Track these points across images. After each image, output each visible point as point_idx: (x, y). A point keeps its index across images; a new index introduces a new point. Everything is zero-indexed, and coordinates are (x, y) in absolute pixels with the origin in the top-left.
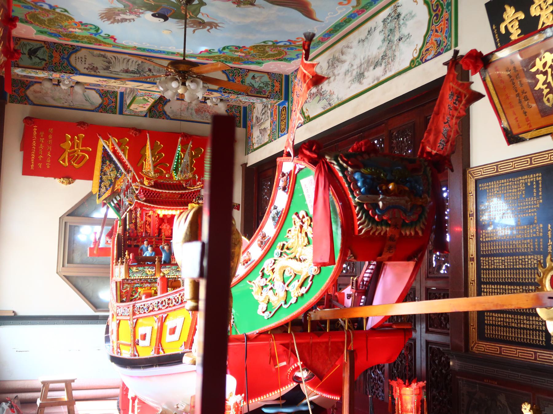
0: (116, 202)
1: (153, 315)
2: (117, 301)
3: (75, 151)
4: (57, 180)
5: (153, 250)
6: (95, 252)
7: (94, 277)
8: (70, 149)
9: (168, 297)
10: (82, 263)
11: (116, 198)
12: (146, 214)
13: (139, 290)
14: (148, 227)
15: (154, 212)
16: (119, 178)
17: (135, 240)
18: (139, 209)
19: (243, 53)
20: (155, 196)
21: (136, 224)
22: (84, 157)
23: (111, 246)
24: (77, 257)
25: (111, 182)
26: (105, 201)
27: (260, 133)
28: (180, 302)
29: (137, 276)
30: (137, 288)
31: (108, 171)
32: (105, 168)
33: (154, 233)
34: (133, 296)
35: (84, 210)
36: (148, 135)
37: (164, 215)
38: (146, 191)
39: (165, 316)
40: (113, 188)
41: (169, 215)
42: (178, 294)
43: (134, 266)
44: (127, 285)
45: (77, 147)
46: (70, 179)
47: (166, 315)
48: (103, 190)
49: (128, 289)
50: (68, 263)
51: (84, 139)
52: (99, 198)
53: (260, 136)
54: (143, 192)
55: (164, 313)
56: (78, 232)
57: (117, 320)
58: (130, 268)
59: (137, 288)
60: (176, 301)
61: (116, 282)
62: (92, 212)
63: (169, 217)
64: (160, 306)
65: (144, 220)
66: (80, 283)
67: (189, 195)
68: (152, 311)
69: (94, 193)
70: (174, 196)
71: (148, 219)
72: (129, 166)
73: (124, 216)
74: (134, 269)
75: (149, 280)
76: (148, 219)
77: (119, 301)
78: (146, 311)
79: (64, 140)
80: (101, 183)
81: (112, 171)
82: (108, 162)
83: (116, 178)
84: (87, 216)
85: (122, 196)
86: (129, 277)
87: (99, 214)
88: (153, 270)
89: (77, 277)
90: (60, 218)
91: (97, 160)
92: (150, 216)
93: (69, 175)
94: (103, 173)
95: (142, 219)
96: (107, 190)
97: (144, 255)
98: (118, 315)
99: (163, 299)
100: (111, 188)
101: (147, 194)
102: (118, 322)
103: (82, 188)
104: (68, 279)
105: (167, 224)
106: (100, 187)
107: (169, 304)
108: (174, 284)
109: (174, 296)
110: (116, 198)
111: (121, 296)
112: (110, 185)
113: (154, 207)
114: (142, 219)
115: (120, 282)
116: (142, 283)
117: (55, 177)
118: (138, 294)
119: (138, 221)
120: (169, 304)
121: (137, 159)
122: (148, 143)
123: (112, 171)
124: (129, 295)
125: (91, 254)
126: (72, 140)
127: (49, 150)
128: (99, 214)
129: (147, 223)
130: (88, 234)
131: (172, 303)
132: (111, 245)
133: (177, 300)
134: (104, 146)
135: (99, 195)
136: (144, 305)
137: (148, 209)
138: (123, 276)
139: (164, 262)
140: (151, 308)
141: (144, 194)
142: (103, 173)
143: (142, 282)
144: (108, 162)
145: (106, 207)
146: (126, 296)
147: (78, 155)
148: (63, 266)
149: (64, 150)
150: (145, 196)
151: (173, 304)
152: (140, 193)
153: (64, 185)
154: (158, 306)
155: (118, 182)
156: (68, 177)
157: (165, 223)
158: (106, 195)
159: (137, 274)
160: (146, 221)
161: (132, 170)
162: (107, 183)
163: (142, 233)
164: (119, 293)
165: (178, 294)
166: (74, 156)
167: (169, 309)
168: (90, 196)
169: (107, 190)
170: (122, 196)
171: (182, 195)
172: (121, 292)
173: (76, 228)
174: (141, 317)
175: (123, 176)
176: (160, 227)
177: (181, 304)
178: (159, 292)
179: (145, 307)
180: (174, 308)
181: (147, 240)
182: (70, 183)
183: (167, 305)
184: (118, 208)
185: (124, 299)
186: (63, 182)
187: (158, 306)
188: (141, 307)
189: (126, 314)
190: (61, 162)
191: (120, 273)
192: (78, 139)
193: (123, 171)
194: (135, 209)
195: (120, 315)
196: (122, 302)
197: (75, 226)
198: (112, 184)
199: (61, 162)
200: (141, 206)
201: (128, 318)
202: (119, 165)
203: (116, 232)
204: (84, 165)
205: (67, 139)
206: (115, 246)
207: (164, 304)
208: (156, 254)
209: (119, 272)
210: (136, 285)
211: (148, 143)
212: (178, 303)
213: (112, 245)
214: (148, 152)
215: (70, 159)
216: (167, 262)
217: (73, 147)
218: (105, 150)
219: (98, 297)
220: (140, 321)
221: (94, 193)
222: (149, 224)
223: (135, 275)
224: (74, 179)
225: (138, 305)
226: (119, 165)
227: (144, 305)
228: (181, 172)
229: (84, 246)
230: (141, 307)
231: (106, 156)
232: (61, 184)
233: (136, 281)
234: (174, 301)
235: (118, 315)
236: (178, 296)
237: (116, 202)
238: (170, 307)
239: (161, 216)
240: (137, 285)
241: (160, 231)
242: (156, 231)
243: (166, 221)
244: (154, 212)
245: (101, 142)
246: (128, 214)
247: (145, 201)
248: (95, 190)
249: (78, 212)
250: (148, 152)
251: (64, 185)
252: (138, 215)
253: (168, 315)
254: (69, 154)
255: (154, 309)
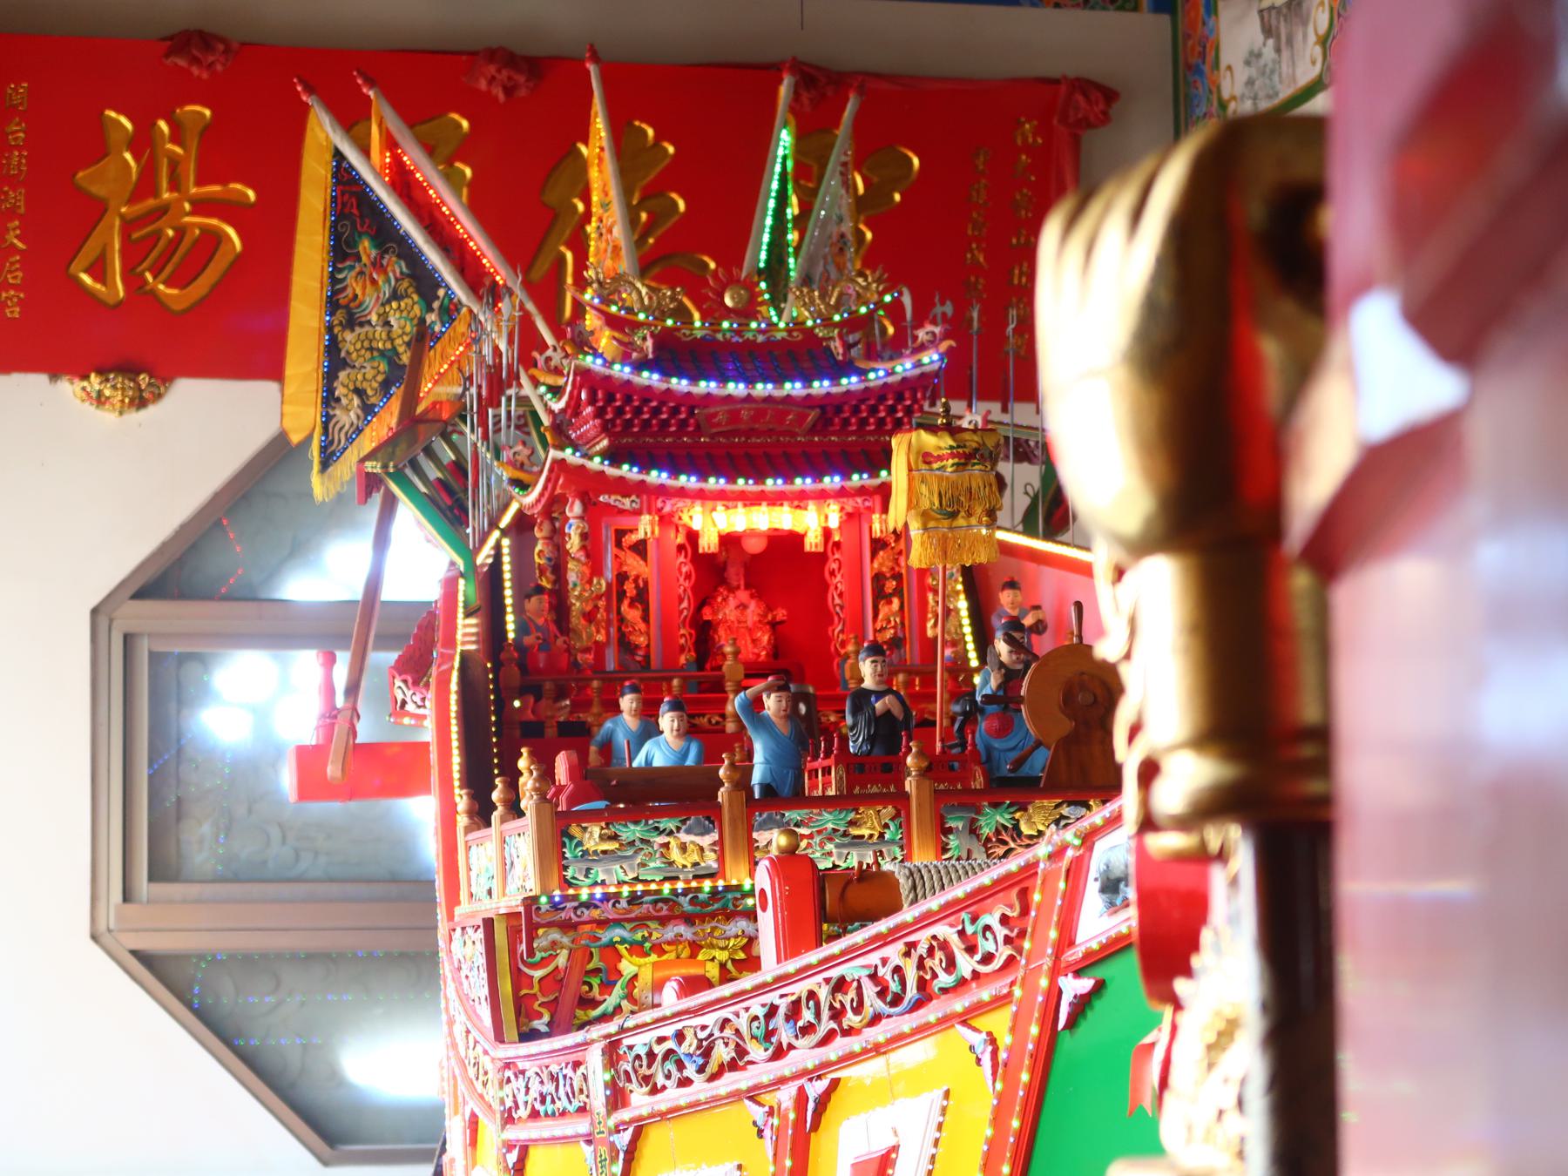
0: (434, 473)
1: (736, 1096)
2: (499, 1037)
3: (162, 211)
4: (68, 388)
5: (690, 731)
6: (333, 770)
7: (310, 958)
8: (134, 198)
9: (834, 973)
10: (232, 876)
11: (429, 452)
12: (620, 534)
13: (628, 967)
14: (633, 615)
15: (666, 520)
16: (437, 338)
17: (560, 694)
18: (577, 508)
19: (650, 298)
20: (665, 424)
21: (559, 601)
22: (212, 240)
23: (428, 734)
24: (201, 842)
25: (394, 364)
26: (373, 467)
27: (1268, 31)
28: (912, 992)
29: (614, 877)
30: (611, 950)
31: (370, 300)
32: (354, 285)
33: (671, 650)
34: (595, 1004)
35: (231, 557)
36: (593, 69)
37: (729, 541)
38: (610, 398)
39: (815, 1089)
40: (411, 399)
41: (752, 533)
42: (900, 946)
43: (594, 816)
44: (555, 935)
45: (174, 186)
46: (144, 379)
47: (820, 1086)
48: (347, 416)
49: (562, 960)
50: (152, 878)
51: (209, 134)
52: (325, 465)
53: (1269, 52)
54: (592, 400)
55: (814, 1074)
56: (205, 692)
57: (510, 1146)
58: (566, 833)
59: (611, 950)
60: (882, 994)
61: (488, 924)
62: (274, 573)
63: (755, 546)
64: (785, 1035)
65: (609, 574)
66: (227, 995)
67: (873, 410)
68: (733, 1066)
69: (295, 438)
70: (780, 416)
71: (634, 565)
72: (491, 259)
73: (484, 557)
74: (592, 837)
75: (684, 901)
76: (634, 565)
77: (511, 1031)
78: (690, 1071)
79: (96, 147)
80: (330, 377)
81: (396, 296)
82: (366, 247)
83: (423, 338)
84: (249, 596)
85: (470, 436)
86: (566, 883)
87: (329, 573)
88: (706, 841)
89: (214, 960)
90: (95, 612)
91: (301, 238)
92: (640, 548)
93: (132, 354)
94: (340, 315)
95: (596, 569)
96: (368, 410)
97: (639, 761)
98: (509, 1119)
99: (800, 989)
100: (395, 405)
101: (619, 412)
102: (512, 1157)
103: (213, 424)
104: (159, 970)
105: (743, 595)
106: (330, 400)
107: (837, 1014)
108: (857, 896)
109: (874, 958)
110: (429, 452)
111: (523, 1009)
112: (386, 386)
113: (662, 491)
114: (596, 569)
115: (511, 916)
116: (640, 922)
117: (55, 373)
118: (618, 990)
119: (572, 577)
120: (837, 1014)
121: (530, 219)
122: (599, 125)
123: (396, 296)
124: (569, 998)
125: (312, 784)
126: (142, 142)
127: (11, 214)
128: (329, 573)
129: (629, 587)
130: (258, 704)
131: (858, 1010)
132: (430, 724)
133: (894, 987)
134: (338, 155)
135: (323, 449)
136: (680, 1037)
137: (626, 503)
138: (525, 878)
139: (767, 788)
140: (723, 1053)
141: (599, 413)
142: (340, 315)
143: (651, 910)
144: (366, 247)
145: (377, 498)
146: (552, 1006)
147: (181, 232)
148: (127, 897)
149: (96, 210)
150: (606, 428)
151: (868, 1011)
152: (575, 407)
153: (107, 418)
154: (769, 1034)
155: (437, 363)
156: (129, 369)
157: (732, 590)
158: (367, 442)
159: (612, 866)
160: (622, 577)
161: (516, 285)
162: (370, 372)
163: (599, 648)
164: (506, 987)
165: (900, 946)
166: (156, 237)
167: (840, 1046)
168: (278, 456)
169: (368, 410)
170: (470, 436)
171: (829, 406)
172: (519, 979)
173: (192, 669)
174: (663, 1116)
175: (461, 327)
176: (707, 615)
177: (918, 1005)
178: (767, 947)
179: (690, 1045)
180: (878, 1034)
181: (634, 689)
182: (140, 402)
183: (826, 1025)
184: (450, 505)
185: (540, 1024)
186: (100, 400)
187: (769, 1034)
188: (659, 1050)
189: (563, 1103)
190: (86, 279)
191: (505, 867)
192: (176, 137)
193: (460, 293)
194: (553, 506)
195: (523, 1112)
196: (528, 1036)
197: (183, 659)
198: (402, 375)
199: (86, 279)
200: (589, 486)
201: (582, 1126)
202: (433, 257)
203: (450, 642)
204: (217, 289)
205: (113, 137)
206: (454, 728)
207: (808, 1015)
208: (711, 756)
209: (503, 866)
210: (607, 935)
211: (599, 125)
212: (897, 1000)
213: (427, 720)
214: (602, 177)
215: (133, 255)
216: (786, 791)
217: (146, 186)
218: (343, 175)
219: (335, 1076)
220: (656, 1138)
221: (295, 438)
222: (641, 598)
223: (599, 873)
224: (165, 376)
225: (640, 1043)
226: (433, 257)
227: (680, 1037)
228: (806, 280)
229: (247, 773)
230: (659, 1050)
231: (353, 208)
232: (89, 408)
233: (608, 911)
234: (870, 990)
235: (509, 1119)
236: (897, 960)
237: (434, 473)
238: (849, 1032)
239: (709, 542)
240: (616, 933)
241: (704, 633)
242: (684, 635)
243: (735, 574)
244: (666, 520)
245: (323, 130)
246: (506, 542)
247: (614, 456)
248: (303, 419)
249: (189, 585)
250: (602, 177)
251: (108, 417)
252: (574, 543)
253: (835, 1083)
254: (128, 226)
255: (741, 1052)
